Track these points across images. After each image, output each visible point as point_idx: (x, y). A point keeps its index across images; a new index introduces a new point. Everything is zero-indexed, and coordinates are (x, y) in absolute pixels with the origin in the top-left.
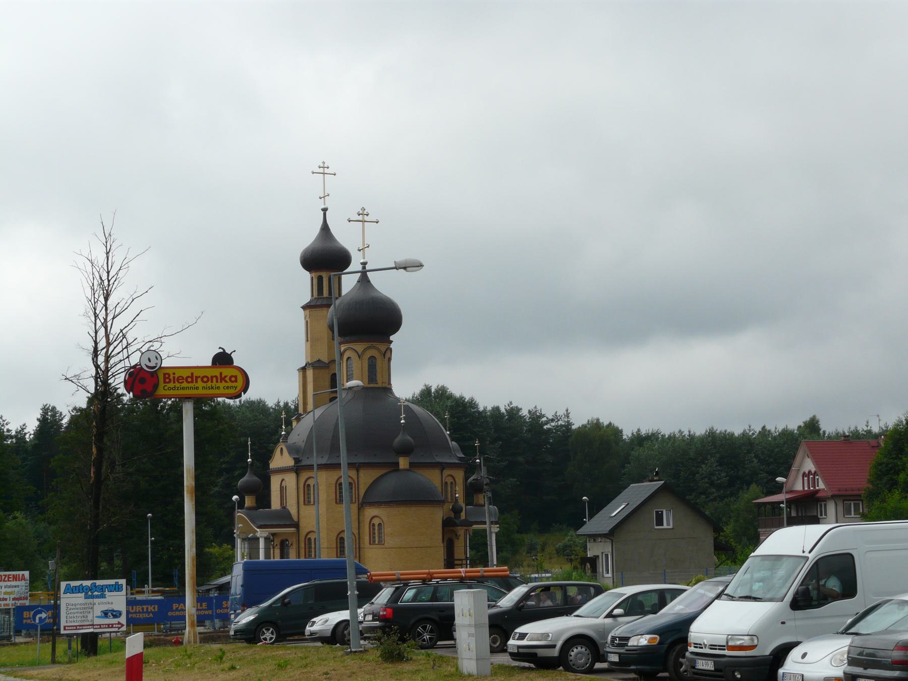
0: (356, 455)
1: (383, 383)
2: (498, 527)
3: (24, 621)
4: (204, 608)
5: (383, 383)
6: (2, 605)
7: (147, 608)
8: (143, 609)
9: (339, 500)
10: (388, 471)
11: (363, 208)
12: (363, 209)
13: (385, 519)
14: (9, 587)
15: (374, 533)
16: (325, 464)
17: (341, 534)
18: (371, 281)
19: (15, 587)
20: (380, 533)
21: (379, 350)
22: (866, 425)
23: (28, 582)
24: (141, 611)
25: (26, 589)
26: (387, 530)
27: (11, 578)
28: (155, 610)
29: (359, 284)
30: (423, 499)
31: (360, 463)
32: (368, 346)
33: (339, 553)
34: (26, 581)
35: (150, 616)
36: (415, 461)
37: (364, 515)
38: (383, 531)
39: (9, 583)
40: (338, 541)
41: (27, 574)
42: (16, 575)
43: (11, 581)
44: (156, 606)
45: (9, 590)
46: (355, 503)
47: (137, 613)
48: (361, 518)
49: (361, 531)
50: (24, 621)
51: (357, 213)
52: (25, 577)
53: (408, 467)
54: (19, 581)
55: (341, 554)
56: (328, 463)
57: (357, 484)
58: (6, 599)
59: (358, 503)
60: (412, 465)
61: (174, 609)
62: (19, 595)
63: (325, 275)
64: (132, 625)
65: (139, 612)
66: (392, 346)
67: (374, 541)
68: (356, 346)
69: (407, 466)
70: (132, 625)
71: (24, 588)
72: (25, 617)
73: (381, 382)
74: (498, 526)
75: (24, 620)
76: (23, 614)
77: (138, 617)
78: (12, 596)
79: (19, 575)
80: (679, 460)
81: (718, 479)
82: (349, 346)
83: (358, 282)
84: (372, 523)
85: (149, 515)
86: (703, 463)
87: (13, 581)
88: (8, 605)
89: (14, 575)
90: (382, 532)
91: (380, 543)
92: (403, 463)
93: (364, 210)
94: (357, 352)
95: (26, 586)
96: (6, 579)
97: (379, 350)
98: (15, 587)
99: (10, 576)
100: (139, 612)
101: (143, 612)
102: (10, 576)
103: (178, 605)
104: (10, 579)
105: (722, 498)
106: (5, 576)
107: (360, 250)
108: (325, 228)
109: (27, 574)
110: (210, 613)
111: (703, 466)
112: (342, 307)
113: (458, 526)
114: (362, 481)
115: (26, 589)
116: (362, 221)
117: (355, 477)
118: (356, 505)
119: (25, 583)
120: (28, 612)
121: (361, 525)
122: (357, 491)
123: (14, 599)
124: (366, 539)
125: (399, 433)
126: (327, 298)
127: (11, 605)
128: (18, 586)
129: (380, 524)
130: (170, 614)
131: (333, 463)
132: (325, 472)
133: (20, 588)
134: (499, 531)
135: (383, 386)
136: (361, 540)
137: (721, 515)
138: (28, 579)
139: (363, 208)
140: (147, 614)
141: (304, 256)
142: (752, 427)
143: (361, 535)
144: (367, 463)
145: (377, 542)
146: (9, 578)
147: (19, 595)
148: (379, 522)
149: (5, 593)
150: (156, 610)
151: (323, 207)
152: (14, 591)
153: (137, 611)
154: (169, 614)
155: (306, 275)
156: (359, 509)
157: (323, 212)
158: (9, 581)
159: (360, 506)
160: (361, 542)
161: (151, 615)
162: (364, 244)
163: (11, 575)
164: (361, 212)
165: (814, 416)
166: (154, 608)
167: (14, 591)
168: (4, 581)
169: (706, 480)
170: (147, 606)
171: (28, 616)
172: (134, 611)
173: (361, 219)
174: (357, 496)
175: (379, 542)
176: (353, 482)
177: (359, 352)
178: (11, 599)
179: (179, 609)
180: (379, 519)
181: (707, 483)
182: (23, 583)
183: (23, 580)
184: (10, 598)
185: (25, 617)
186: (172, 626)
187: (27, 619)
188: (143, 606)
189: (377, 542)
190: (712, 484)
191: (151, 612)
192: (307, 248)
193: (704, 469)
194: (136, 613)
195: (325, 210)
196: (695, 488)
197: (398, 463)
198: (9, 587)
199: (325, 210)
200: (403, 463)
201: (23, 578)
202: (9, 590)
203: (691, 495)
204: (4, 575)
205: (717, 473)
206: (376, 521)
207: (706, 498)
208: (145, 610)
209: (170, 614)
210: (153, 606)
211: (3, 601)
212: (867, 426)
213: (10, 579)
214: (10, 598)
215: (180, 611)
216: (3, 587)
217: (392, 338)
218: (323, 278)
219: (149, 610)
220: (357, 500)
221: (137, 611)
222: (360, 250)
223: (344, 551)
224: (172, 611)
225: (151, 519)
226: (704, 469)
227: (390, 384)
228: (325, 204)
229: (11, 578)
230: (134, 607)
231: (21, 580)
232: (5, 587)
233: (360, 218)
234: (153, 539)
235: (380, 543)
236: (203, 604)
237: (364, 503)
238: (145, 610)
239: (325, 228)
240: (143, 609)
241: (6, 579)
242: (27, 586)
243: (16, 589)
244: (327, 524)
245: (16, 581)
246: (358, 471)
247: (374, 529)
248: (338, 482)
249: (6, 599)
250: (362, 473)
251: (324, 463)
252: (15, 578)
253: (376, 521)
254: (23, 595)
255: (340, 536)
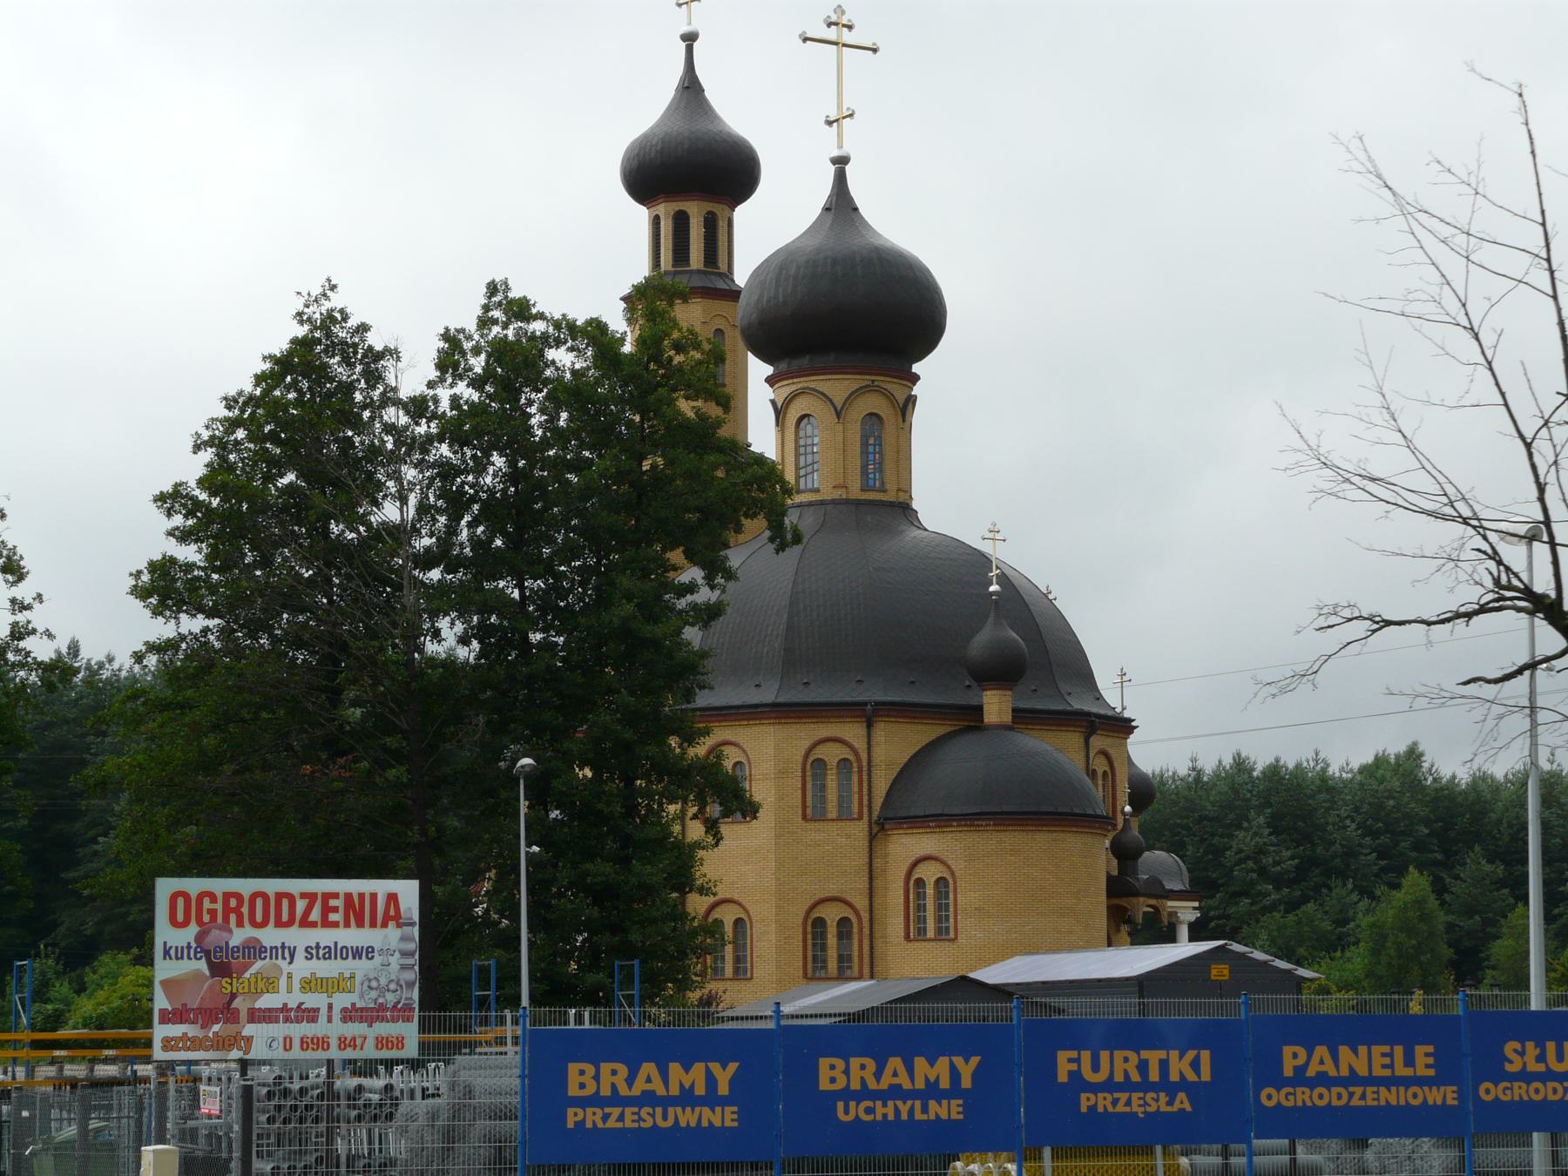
0: (859, 681)
1: (898, 490)
2: (1195, 908)
3: (572, 1116)
4: (1422, 1071)
5: (898, 490)
6: (334, 1043)
7: (1164, 1065)
8: (1143, 1067)
9: (813, 813)
10: (949, 729)
11: (839, 6)
12: (840, 10)
13: (958, 865)
14: (330, 953)
15: (921, 908)
16: (774, 705)
17: (820, 908)
18: (861, 210)
19: (357, 953)
20: (941, 908)
21: (889, 397)
22: (1549, 761)
23: (416, 931)
24: (1135, 1077)
25: (404, 967)
26: (966, 897)
27: (335, 909)
28: (1198, 1073)
29: (830, 217)
30: (1034, 809)
31: (878, 704)
32: (864, 384)
33: (810, 965)
34: (407, 929)
35: (1176, 1106)
36: (1039, 707)
37: (886, 855)
38: (951, 901)
39: (325, 937)
40: (809, 929)
41: (408, 891)
42: (362, 896)
43: (335, 925)
44: (1205, 1055)
45: (327, 969)
46: (860, 818)
47: (1121, 1087)
48: (878, 862)
49: (877, 901)
50: (572, 1116)
51: (825, 20)
52: (403, 907)
53: (1010, 720)
54: (373, 924)
55: (815, 969)
56: (781, 700)
57: (865, 764)
58: (311, 1015)
59: (870, 813)
60: (1023, 718)
61: (1288, 1072)
62: (374, 994)
63: (696, 211)
64: (1047, 1152)
65: (1127, 1086)
66: (916, 390)
67: (922, 931)
68: (829, 383)
69: (1007, 718)
70: (1047, 1152)
71: (395, 961)
72: (573, 1091)
73: (895, 487)
74: (1196, 904)
75: (570, 1111)
76: (564, 1076)
77: (1120, 1108)
78: (342, 1001)
79: (374, 896)
80: (1179, 821)
81: (1278, 863)
82: (806, 385)
83: (827, 209)
84: (915, 876)
85: (527, 761)
86: (1239, 827)
87: (347, 925)
88: (321, 1043)
89: (348, 896)
90: (947, 905)
91: (942, 933)
92: (996, 706)
93: (843, 12)
94: (831, 401)
95: (404, 954)
96: (315, 915)
97: (889, 397)
98: (357, 953)
99: (333, 903)
100: (1127, 1086)
101: (1145, 1086)
102: (333, 903)
103: (1302, 1053)
104: (333, 917)
105: (1292, 906)
106: (311, 897)
107: (830, 123)
108: (691, 87)
109: (408, 891)
110: (1449, 1102)
111: (1241, 834)
112: (792, 272)
113: (1136, 894)
114: (880, 754)
115: (404, 967)
116: (836, 43)
117: (860, 745)
118: (863, 825)
119: (403, 939)
120: (590, 1069)
121: (878, 883)
122: (865, 784)
123: (350, 1015)
124: (894, 925)
125: (987, 616)
126: (699, 271)
127: (334, 1043)
128: (369, 952)
129: (941, 882)
130: (1271, 1097)
131: (795, 700)
132: (771, 728)
133: (378, 960)
134: (1197, 918)
135: (901, 500)
136: (876, 926)
137: (1292, 943)
138: (416, 918)
139: (839, 6)
140: (1163, 1097)
141: (629, 159)
142: (1322, 756)
143: (876, 911)
144: (892, 704)
145: (930, 934)
146: (327, 910)
147: (374, 994)
148: (939, 875)
149: (309, 984)
150: (1206, 1075)
151: (685, 29)
152: (352, 977)
153: (606, 1091)
154: (1482, 1094)
155: (638, 217)
156: (872, 838)
157: (683, 45)
158: (326, 924)
159: (875, 830)
160: (877, 934)
161: (1182, 1102)
162: (840, 106)
163: (336, 896)
164: (834, 18)
165: (1415, 744)
166: (1195, 1065)
167: (352, 977)
168: (305, 923)
169: (1251, 864)
170: (1162, 1054)
171: (590, 1090)
172: (1101, 1077)
173: (833, 37)
174: (865, 798)
175: (939, 931)
176: (852, 758)
177: (835, 400)
178: (336, 1015)
179: (1311, 1073)
180: (938, 864)
181: (1252, 871)
182: (392, 934)
183: (391, 924)
184: (330, 1007)
185: (573, 1091)
186: (1256, 1159)
187: (583, 1102)
188: (1145, 1054)
189: (930, 934)
190: (1263, 872)
191: (1183, 1084)
192: (645, 136)
193: (1243, 840)
194: (1109, 1086)
195: (690, 38)
196: (1220, 882)
197: (979, 709)
198: (330, 953)
199: (690, 38)
200: (996, 706)
201: (392, 913)
202: (327, 969)
203: (1212, 897)
204: (303, 895)
205: (1272, 848)
206: (929, 873)
207: (1251, 904)
208: (1154, 1076)
209: (1271, 1097)
210: (1191, 1054)
211: (298, 1021)
212: (1552, 763)
213: (333, 917)
214: (330, 1007)
215: (1312, 1083)
216: (300, 955)
217: (917, 368)
218: (688, 218)
219: (1174, 1077)
220: (865, 810)
221: (1119, 1078)
222: (830, 123)
223: (825, 961)
224: (1279, 1082)
225: (529, 775)
226: (1243, 840)
227: (908, 491)
228: (690, 24)
229: (335, 909)
230: (1104, 1056)
231: (384, 925)
232: (310, 953)
233: (831, 34)
234: (536, 849)
235: (942, 933)
236: (1421, 1050)
237: (886, 819)
238: (1154, 1076)
239: (691, 87)
240: (1143, 1067)
241: (315, 915)
242: (412, 954)
243: (361, 967)
244: (778, 879)
245: (360, 924)
246: (869, 726)
247: (921, 896)
248: (811, 759)
249: (311, 1015)
250: (882, 731)
251: (770, 701)
252: (356, 912)
253: (929, 873)
254: (390, 998)
255: (815, 914)
